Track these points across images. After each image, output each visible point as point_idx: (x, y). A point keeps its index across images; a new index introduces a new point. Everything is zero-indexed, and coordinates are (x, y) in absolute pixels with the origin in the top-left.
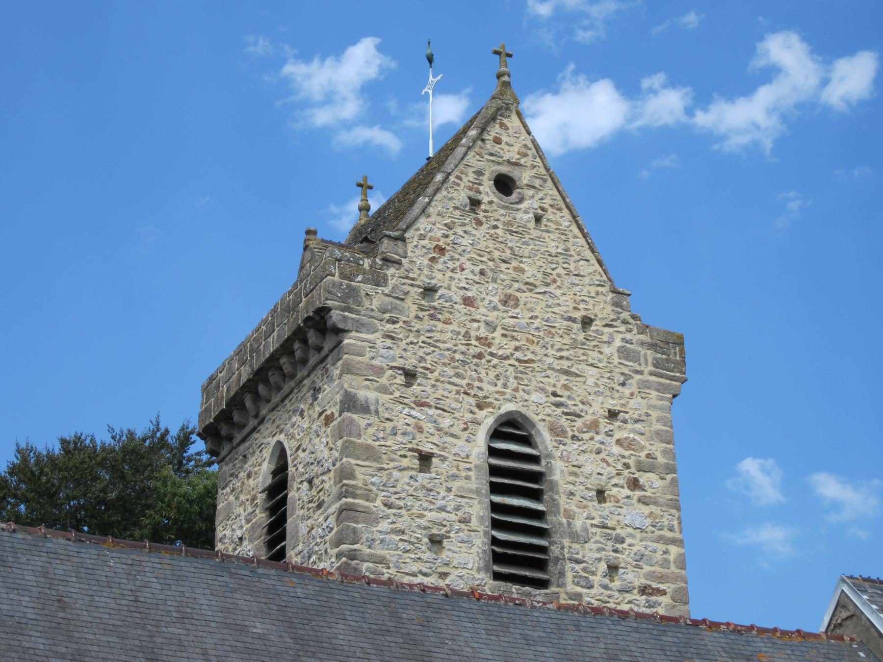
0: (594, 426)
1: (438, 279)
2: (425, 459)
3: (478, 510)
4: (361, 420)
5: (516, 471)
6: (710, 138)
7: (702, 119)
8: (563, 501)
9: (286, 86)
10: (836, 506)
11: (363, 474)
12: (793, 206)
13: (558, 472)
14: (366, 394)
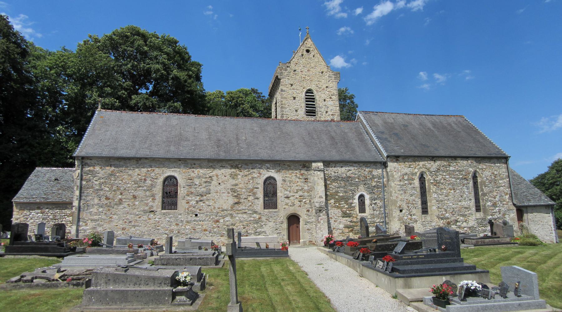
0: (324, 89)
1: (296, 68)
2: (294, 98)
3: (303, 105)
4: (283, 93)
5: (310, 97)
6: (410, 9)
7: (408, 5)
8: (318, 102)
9: (325, 7)
10: (438, 79)
11: (284, 101)
12: (428, 21)
13: (317, 97)
14: (284, 89)
